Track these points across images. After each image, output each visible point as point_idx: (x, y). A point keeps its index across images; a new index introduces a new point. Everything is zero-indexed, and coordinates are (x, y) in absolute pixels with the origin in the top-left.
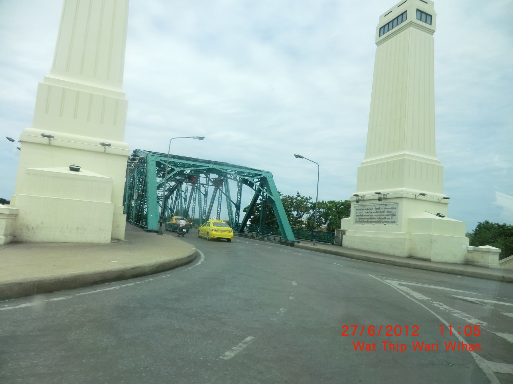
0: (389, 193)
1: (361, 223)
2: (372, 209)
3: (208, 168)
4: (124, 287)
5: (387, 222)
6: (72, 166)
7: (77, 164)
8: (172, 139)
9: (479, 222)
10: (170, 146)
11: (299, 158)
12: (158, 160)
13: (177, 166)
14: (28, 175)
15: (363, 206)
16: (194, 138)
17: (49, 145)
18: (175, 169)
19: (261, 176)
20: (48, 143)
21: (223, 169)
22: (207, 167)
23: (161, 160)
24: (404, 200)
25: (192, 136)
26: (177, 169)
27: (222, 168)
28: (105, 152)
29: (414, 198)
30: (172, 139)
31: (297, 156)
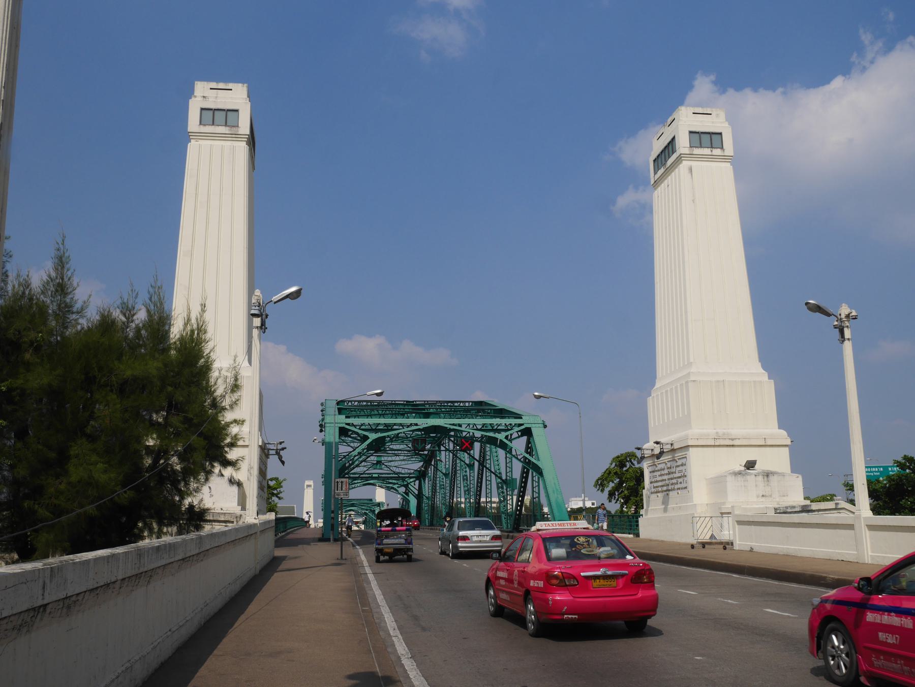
2: (663, 469)
5: (679, 489)
21: (453, 425)
26: (373, 436)
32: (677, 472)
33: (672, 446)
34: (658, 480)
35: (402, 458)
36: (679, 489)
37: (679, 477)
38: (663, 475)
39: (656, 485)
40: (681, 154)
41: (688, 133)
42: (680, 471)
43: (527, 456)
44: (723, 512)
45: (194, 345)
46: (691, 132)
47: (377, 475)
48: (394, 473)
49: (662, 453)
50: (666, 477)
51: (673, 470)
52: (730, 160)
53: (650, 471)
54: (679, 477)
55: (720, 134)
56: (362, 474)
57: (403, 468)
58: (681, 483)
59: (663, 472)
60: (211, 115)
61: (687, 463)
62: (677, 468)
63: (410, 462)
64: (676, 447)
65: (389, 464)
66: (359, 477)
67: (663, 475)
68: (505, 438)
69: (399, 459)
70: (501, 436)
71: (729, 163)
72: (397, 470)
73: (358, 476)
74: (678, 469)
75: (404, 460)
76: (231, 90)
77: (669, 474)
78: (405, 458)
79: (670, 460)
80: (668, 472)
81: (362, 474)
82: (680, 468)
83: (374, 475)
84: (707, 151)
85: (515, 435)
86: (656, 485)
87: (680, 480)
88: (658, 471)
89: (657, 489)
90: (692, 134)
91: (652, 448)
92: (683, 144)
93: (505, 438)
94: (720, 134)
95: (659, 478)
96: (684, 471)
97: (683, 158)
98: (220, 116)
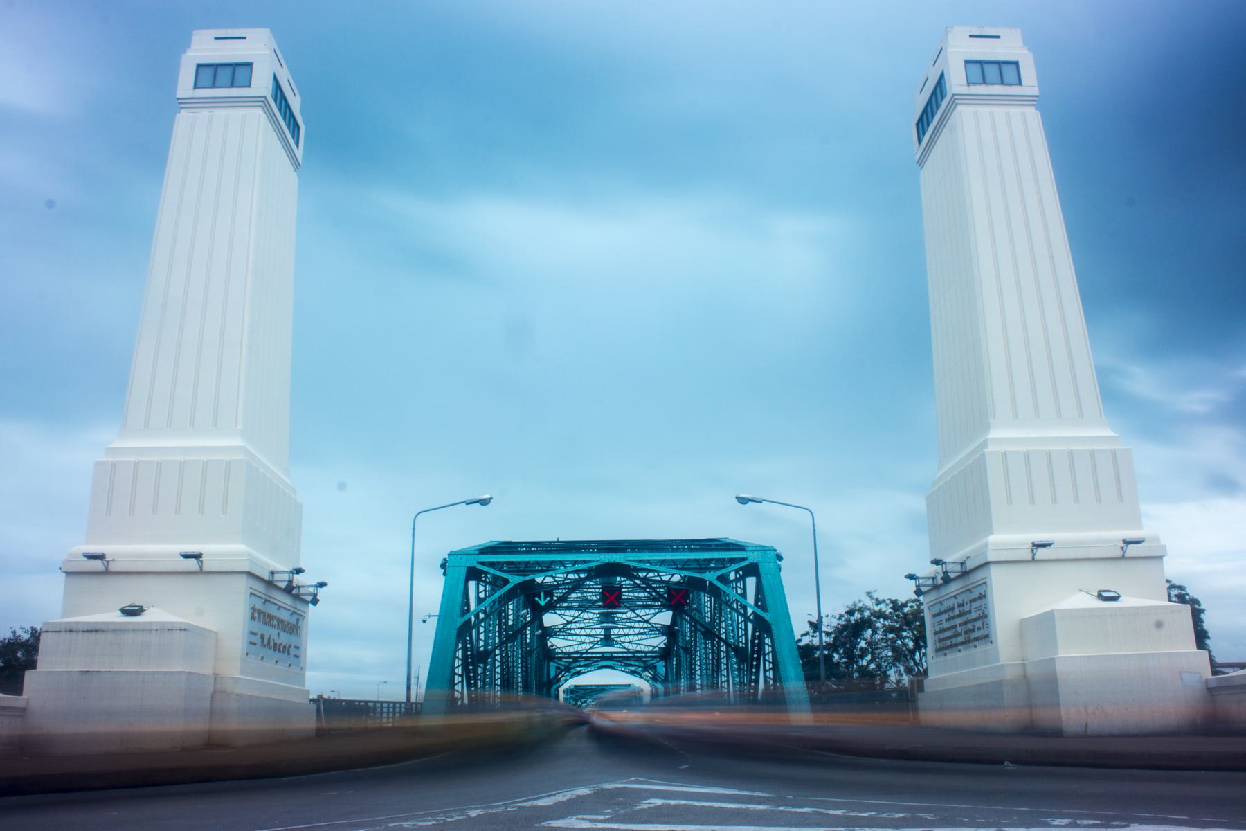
0: (968, 555)
1: (954, 649)
2: (952, 609)
3: (598, 563)
4: (900, 818)
5: (976, 639)
6: (130, 606)
7: (1113, 587)
8: (812, 513)
9: (14, 632)
10: (412, 531)
11: (750, 503)
12: (473, 563)
13: (703, 569)
14: (57, 633)
15: (939, 605)
16: (467, 504)
17: (201, 572)
18: (510, 580)
19: (745, 563)
20: (198, 569)
21: (640, 561)
22: (594, 561)
23: (482, 563)
24: (993, 568)
25: (463, 501)
26: (515, 580)
27: (636, 558)
28: (1123, 556)
29: (1030, 557)
30: (812, 513)
31: (743, 501)
32: (973, 610)
33: (962, 566)
34: (945, 627)
35: (637, 631)
36: (976, 639)
37: (977, 619)
38: (953, 618)
39: (942, 636)
40: (954, 95)
41: (963, 63)
42: (978, 609)
43: (759, 612)
44: (966, 82)
45: (533, 549)
46: (967, 62)
47: (609, 655)
48: (628, 652)
49: (947, 580)
50: (958, 621)
51: (966, 608)
52: (1035, 103)
53: (934, 613)
54: (977, 619)
55: (1016, 64)
56: (584, 653)
57: (637, 644)
58: (979, 629)
59: (951, 614)
60: (210, 73)
61: (989, 594)
62: (972, 604)
63: (652, 636)
64: (970, 566)
65: (622, 639)
66: (581, 657)
67: (953, 618)
68: (716, 579)
69: (633, 633)
70: (710, 577)
71: (1033, 107)
72: (630, 647)
73: (579, 655)
74: (974, 605)
75: (639, 634)
76: (245, 38)
77: (961, 615)
78: (642, 631)
79: (961, 591)
80: (960, 611)
81: (584, 653)
82: (978, 604)
83: (605, 655)
84: (998, 89)
85: (732, 576)
86: (942, 636)
87: (978, 624)
88: (945, 612)
89: (944, 643)
90: (969, 66)
91: (933, 576)
92: (957, 82)
93: (716, 579)
94: (1016, 64)
95: (946, 625)
96: (983, 608)
97: (957, 101)
98: (224, 75)
